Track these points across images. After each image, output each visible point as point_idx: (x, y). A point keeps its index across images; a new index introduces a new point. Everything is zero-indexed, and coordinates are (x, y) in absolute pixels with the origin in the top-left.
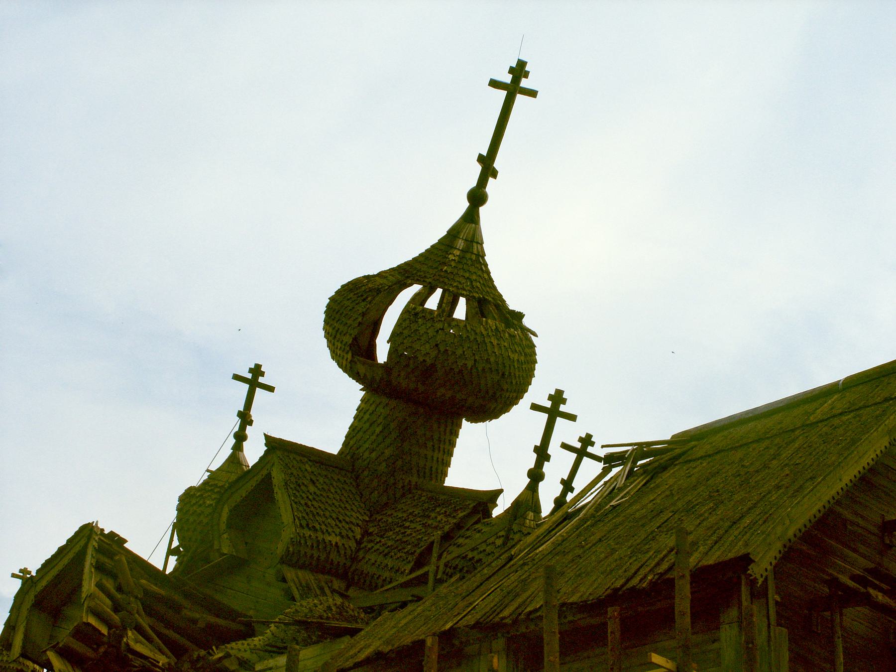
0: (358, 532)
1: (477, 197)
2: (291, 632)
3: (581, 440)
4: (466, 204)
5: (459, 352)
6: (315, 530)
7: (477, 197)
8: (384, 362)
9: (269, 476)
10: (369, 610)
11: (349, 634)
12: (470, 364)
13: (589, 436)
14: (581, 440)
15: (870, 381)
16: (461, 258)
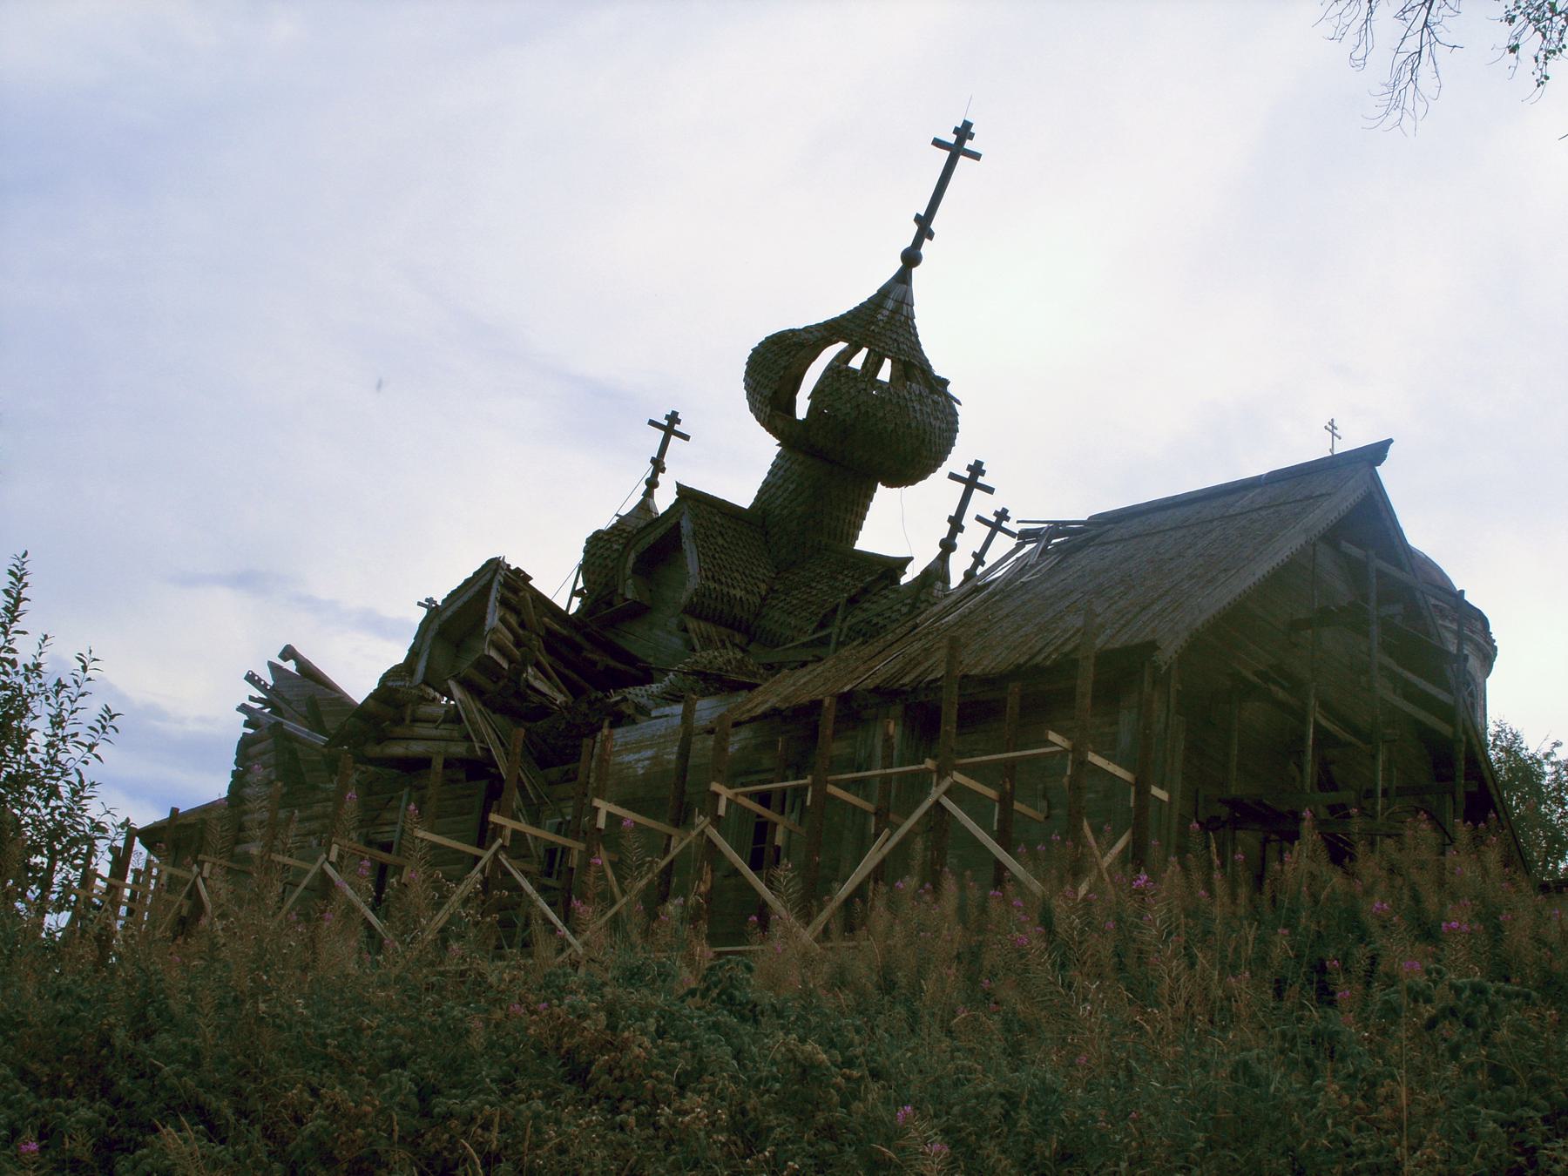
0: (763, 587)
1: (911, 258)
3: (996, 514)
4: (898, 264)
7: (911, 258)
9: (677, 526)
14: (996, 514)
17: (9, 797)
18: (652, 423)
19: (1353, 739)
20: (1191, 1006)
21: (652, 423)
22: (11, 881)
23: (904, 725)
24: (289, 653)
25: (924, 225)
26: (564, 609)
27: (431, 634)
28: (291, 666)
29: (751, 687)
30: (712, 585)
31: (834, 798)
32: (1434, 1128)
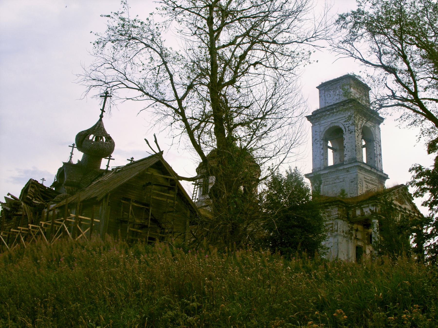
0: (80, 179)
1: (101, 116)
2: (203, 10)
3: (131, 158)
4: (99, 118)
5: (94, 147)
6: (70, 179)
7: (101, 116)
8: (79, 161)
9: (64, 169)
10: (402, 24)
11: (425, 218)
12: (96, 149)
13: (133, 158)
14: (131, 158)
15: (358, 51)
16: (98, 128)
17: (287, 199)
18: (69, 146)
19: (143, 206)
20: (257, 271)
21: (69, 146)
22: (381, 294)
23: (378, 168)
24: (9, 194)
25: (103, 111)
26: (155, 153)
27: (23, 192)
28: (9, 197)
29: (60, 202)
30: (69, 180)
31: (68, 221)
32: (76, 266)
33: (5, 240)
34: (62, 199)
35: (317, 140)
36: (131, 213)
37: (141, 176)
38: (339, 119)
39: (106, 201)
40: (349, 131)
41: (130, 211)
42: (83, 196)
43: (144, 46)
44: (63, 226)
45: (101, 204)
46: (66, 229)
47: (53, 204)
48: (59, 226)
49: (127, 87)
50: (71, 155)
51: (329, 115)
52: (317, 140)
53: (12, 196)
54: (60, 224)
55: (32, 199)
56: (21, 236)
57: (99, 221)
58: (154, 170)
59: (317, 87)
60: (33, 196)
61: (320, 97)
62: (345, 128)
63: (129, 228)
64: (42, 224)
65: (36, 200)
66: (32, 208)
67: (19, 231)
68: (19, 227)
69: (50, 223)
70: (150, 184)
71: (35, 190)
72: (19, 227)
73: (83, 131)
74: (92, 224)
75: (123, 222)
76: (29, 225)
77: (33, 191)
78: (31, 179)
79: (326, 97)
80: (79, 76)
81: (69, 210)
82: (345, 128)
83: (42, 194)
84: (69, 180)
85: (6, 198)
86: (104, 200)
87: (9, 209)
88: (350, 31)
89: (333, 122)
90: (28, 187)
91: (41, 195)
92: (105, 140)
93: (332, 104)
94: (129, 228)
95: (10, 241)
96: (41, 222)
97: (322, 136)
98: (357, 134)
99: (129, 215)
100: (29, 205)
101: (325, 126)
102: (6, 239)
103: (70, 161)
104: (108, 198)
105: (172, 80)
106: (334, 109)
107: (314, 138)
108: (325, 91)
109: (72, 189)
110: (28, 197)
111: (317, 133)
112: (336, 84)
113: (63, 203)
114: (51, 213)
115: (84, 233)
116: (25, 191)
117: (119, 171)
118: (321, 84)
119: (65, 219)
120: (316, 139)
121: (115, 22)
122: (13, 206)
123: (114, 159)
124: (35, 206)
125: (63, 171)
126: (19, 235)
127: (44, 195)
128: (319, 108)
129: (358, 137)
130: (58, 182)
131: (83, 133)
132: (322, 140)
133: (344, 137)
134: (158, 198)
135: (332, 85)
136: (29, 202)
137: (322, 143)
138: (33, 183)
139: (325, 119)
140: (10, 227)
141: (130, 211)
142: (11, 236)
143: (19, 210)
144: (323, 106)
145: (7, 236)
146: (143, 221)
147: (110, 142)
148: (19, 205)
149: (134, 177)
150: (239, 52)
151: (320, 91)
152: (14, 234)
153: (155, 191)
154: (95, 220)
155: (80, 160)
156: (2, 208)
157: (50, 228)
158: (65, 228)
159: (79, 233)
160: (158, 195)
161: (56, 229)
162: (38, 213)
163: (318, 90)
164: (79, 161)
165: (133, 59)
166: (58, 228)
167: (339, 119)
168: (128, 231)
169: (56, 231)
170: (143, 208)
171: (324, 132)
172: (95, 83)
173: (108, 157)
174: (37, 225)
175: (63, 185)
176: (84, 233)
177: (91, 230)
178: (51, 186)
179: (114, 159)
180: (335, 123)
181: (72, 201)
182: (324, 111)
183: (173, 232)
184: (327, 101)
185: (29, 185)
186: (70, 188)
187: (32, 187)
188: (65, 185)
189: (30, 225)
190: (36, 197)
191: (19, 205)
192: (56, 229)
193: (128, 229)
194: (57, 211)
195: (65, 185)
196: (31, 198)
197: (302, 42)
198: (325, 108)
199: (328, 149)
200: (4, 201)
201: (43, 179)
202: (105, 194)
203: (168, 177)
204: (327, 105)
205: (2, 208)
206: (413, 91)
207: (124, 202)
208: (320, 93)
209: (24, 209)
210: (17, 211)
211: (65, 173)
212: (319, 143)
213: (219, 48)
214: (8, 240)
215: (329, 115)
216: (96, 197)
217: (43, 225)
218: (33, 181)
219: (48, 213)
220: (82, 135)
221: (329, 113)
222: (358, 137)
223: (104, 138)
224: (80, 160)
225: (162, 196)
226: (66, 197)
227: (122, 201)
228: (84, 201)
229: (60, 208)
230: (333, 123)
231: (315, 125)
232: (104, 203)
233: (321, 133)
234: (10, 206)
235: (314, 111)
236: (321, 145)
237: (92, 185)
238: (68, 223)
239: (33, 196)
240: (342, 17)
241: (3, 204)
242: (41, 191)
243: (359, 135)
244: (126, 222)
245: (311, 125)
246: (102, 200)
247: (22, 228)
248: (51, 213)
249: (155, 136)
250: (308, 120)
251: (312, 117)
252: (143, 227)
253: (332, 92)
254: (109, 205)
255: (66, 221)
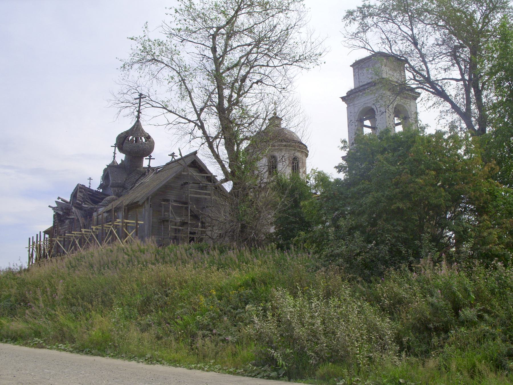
18: (112, 146)
21: (112, 146)
24: (59, 198)
28: (60, 201)
30: (114, 182)
33: (61, 243)
34: (110, 202)
35: (353, 121)
36: (172, 212)
37: (179, 177)
38: (370, 99)
39: (148, 203)
40: (380, 111)
41: (170, 211)
42: (126, 200)
43: (165, 65)
44: (112, 229)
45: (144, 206)
46: (115, 232)
47: (102, 207)
48: (108, 229)
49: (153, 106)
50: (115, 155)
51: (362, 95)
52: (353, 121)
53: (63, 200)
54: (110, 227)
55: (82, 204)
56: (76, 240)
57: (143, 223)
58: (191, 168)
59: (351, 66)
60: (82, 200)
61: (354, 75)
62: (377, 109)
63: (171, 227)
64: (93, 228)
65: (85, 204)
66: (83, 212)
67: (73, 235)
68: (73, 232)
69: (100, 227)
70: (186, 183)
71: (83, 195)
72: (73, 232)
73: (122, 133)
74: (137, 226)
75: (164, 221)
76: (82, 230)
77: (81, 195)
78: (78, 184)
79: (360, 75)
80: (109, 101)
81: (116, 214)
82: (377, 109)
83: (90, 197)
84: (114, 182)
85: (56, 202)
86: (146, 203)
87: (61, 213)
88: (361, 23)
89: (366, 102)
90: (76, 192)
91: (90, 198)
92: (144, 140)
93: (366, 83)
94: (171, 227)
95: (66, 243)
96: (92, 227)
97: (357, 117)
98: (387, 115)
99: (169, 215)
100: (79, 209)
101: (359, 107)
102: (62, 242)
103: (113, 162)
104: (149, 201)
105: (190, 96)
106: (366, 89)
107: (350, 120)
108: (358, 70)
109: (118, 191)
110: (78, 201)
111: (352, 114)
112: (368, 62)
113: (109, 207)
114: (100, 217)
115: (130, 235)
116: (74, 195)
117: (159, 171)
118: (354, 62)
119: (113, 223)
120: (351, 121)
121: (137, 46)
122: (65, 211)
123: (154, 159)
124: (85, 211)
125: (108, 173)
126: (74, 239)
127: (92, 198)
128: (353, 88)
129: (389, 117)
130: (104, 184)
131: (123, 135)
132: (357, 121)
133: (376, 118)
134: (195, 196)
135: (365, 63)
136: (79, 207)
137: (356, 124)
138: (80, 188)
139: (359, 100)
140: (64, 230)
141: (170, 211)
142: (66, 239)
143: (70, 214)
144: (358, 86)
145: (62, 239)
146: (183, 219)
147: (150, 141)
148: (70, 210)
149: (172, 178)
150: (243, 72)
151: (354, 69)
152: (69, 237)
153: (192, 190)
154: (139, 222)
155: (123, 160)
156: (54, 212)
157: (100, 231)
158: (113, 232)
159: (126, 235)
160: (196, 193)
161: (107, 231)
162: (88, 217)
163: (352, 68)
164: (122, 160)
165: (157, 75)
166: (108, 230)
167: (370, 99)
168: (170, 229)
169: (107, 233)
170: (182, 206)
171: (359, 112)
172: (123, 105)
173: (148, 157)
174: (89, 229)
175: (109, 187)
176: (130, 235)
177: (136, 231)
178: (98, 188)
179: (154, 159)
180: (367, 103)
181: (118, 205)
182: (357, 92)
183: (163, 245)
184: (361, 80)
185: (77, 190)
186: (116, 189)
187: (80, 192)
188: (111, 186)
189: (83, 230)
190: (84, 201)
191: (70, 210)
192: (107, 231)
193: (170, 227)
194: (105, 215)
195: (111, 186)
196: (81, 203)
197: (291, 64)
198: (358, 88)
199: (364, 128)
200: (55, 205)
201: (90, 178)
202: (146, 198)
203: (203, 175)
204: (361, 84)
205: (54, 212)
206: (427, 76)
207: (164, 203)
208: (354, 72)
209: (76, 214)
210: (69, 215)
211: (110, 175)
212: (353, 124)
213: (223, 73)
214: (64, 243)
215: (362, 95)
216: (138, 202)
217: (94, 230)
218: (81, 186)
219: (97, 216)
220: (121, 138)
221: (361, 93)
222: (389, 117)
223: (143, 138)
224: (123, 160)
225: (200, 194)
226: (113, 200)
227: (162, 203)
228: (127, 205)
229: (108, 212)
230: (365, 103)
231: (350, 106)
232: (146, 205)
233: (355, 114)
234: (62, 210)
235: (348, 92)
236: (356, 126)
237: (135, 187)
238: (116, 227)
239: (82, 200)
240: (350, 13)
241: (54, 208)
242: (89, 194)
243: (390, 115)
244: (167, 221)
245: (346, 106)
246: (144, 203)
247: (75, 233)
248: (100, 217)
249: (179, 150)
250: (343, 100)
251: (346, 98)
252: (183, 224)
253: (365, 71)
254: (151, 207)
255: (114, 225)
